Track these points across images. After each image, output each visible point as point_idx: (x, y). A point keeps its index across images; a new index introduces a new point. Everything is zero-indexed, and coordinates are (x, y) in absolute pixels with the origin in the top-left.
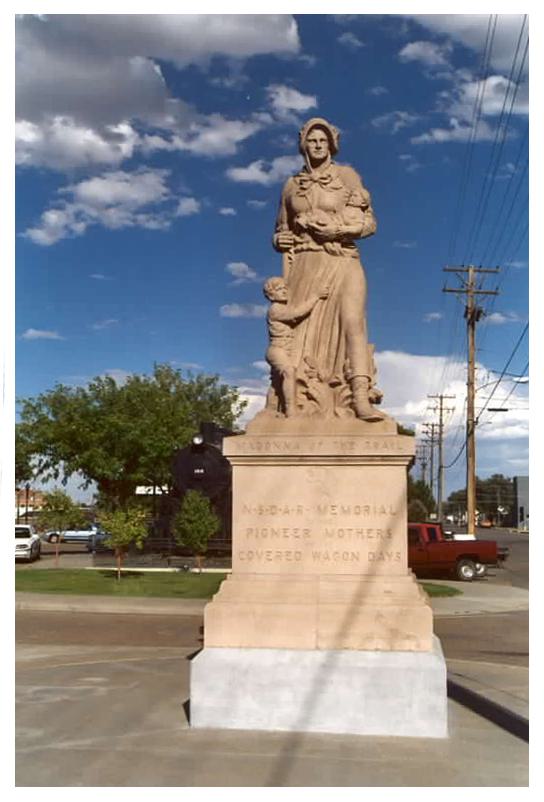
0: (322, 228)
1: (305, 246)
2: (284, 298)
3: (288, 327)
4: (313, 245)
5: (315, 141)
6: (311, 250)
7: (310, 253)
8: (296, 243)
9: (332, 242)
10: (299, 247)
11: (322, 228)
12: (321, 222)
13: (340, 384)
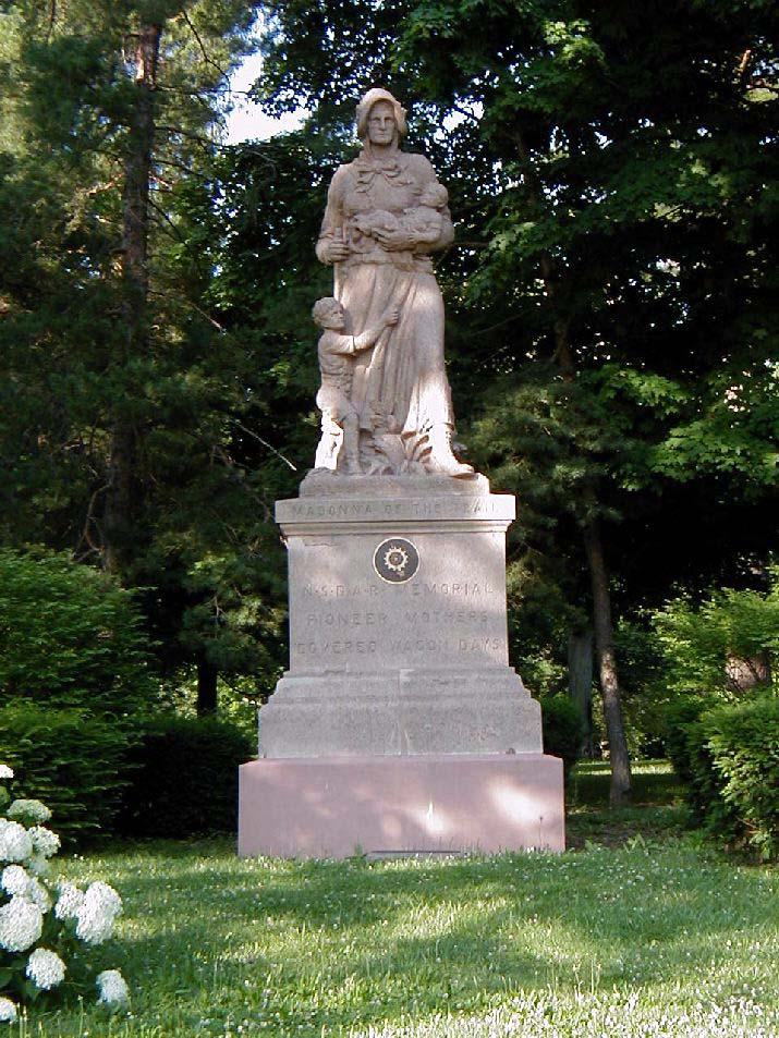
0: (388, 235)
2: (341, 325)
3: (345, 361)
5: (378, 119)
9: (401, 251)
10: (358, 257)
11: (388, 235)
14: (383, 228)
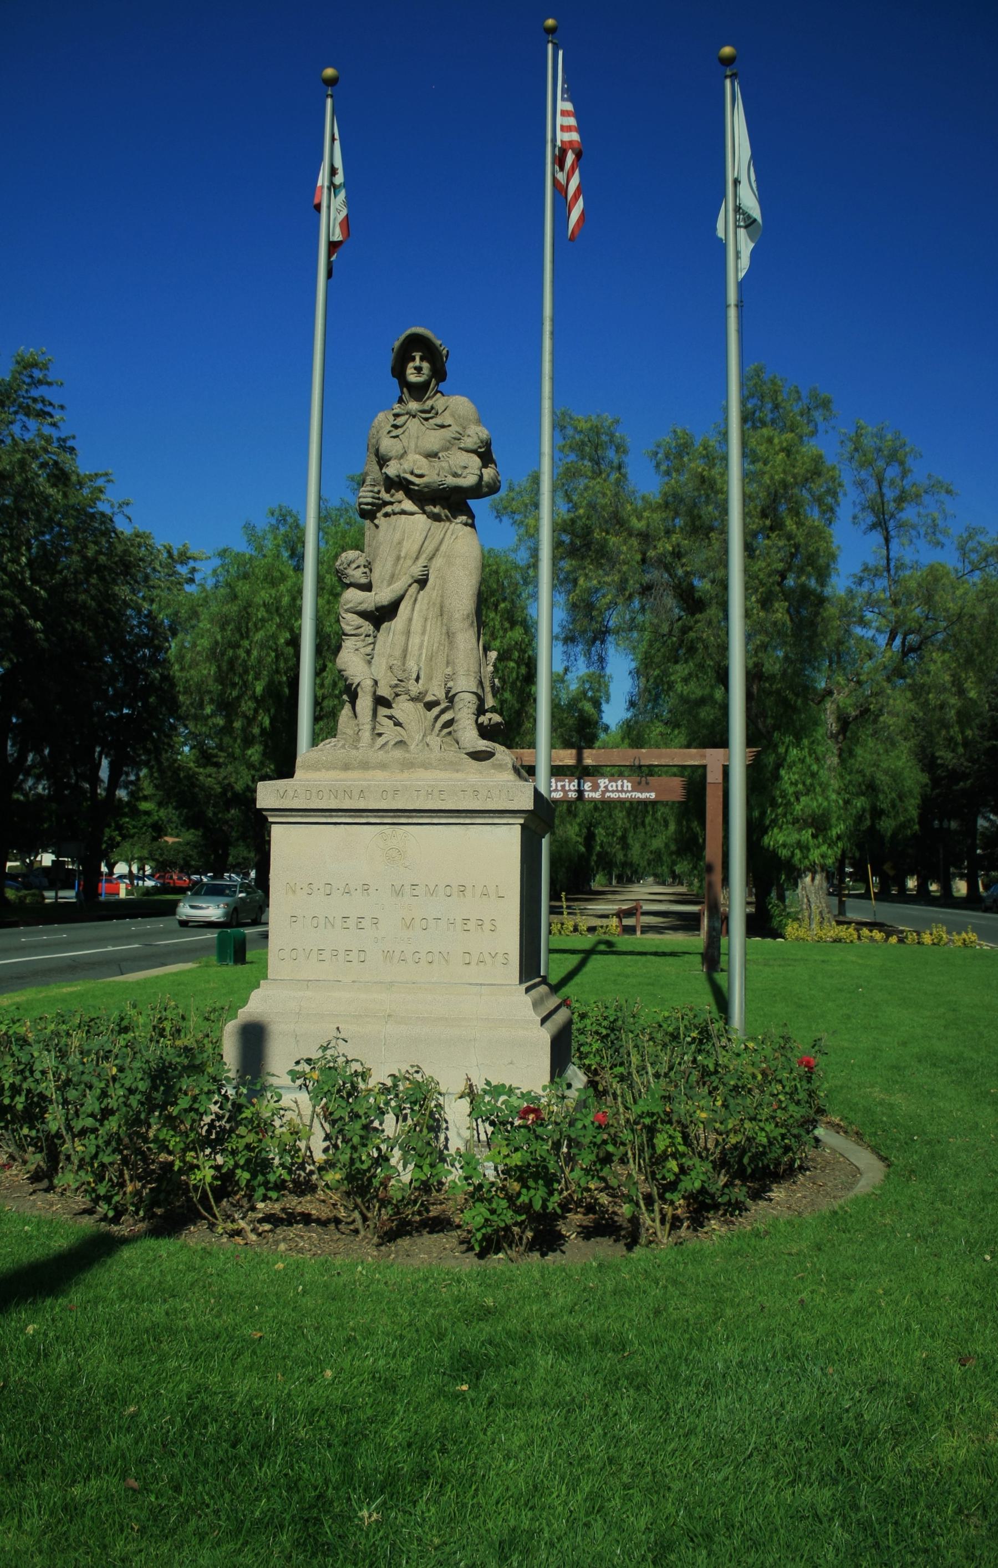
0: (417, 480)
1: (396, 508)
4: (408, 505)
6: (403, 512)
7: (403, 516)
8: (386, 503)
10: (388, 509)
12: (416, 472)
13: (436, 703)
14: (412, 473)
